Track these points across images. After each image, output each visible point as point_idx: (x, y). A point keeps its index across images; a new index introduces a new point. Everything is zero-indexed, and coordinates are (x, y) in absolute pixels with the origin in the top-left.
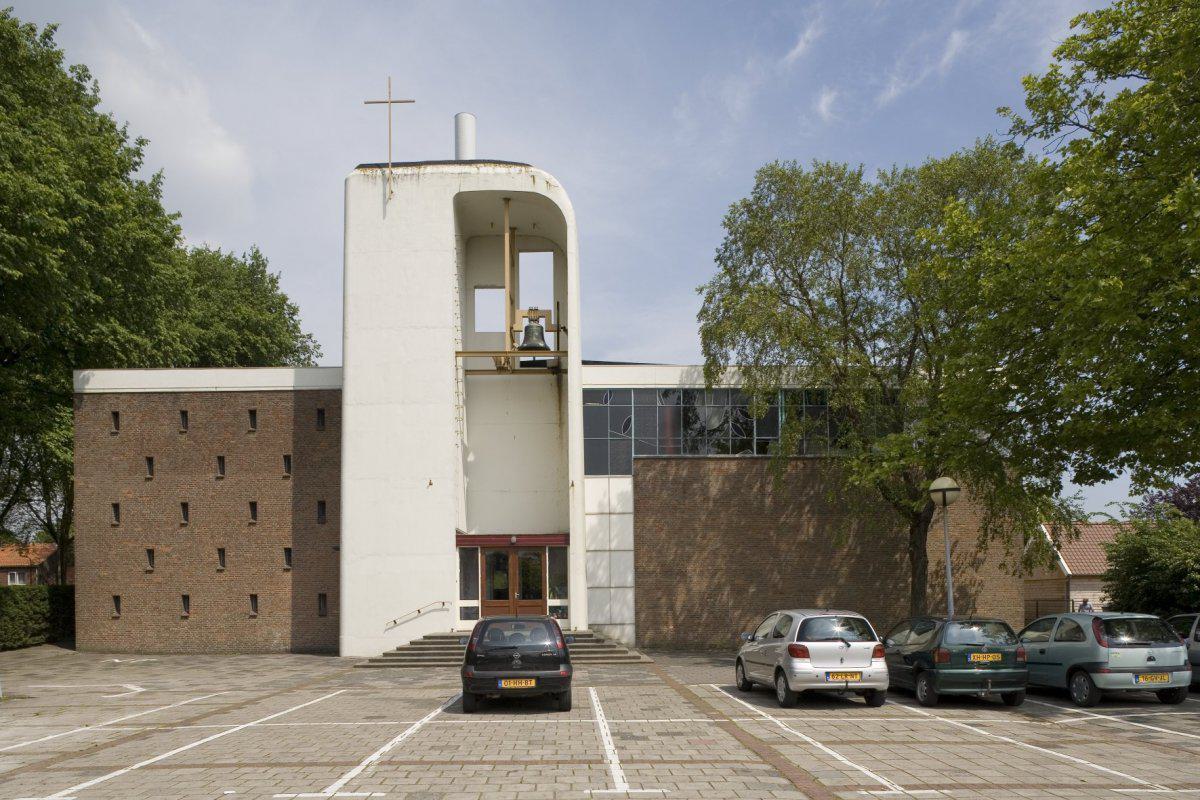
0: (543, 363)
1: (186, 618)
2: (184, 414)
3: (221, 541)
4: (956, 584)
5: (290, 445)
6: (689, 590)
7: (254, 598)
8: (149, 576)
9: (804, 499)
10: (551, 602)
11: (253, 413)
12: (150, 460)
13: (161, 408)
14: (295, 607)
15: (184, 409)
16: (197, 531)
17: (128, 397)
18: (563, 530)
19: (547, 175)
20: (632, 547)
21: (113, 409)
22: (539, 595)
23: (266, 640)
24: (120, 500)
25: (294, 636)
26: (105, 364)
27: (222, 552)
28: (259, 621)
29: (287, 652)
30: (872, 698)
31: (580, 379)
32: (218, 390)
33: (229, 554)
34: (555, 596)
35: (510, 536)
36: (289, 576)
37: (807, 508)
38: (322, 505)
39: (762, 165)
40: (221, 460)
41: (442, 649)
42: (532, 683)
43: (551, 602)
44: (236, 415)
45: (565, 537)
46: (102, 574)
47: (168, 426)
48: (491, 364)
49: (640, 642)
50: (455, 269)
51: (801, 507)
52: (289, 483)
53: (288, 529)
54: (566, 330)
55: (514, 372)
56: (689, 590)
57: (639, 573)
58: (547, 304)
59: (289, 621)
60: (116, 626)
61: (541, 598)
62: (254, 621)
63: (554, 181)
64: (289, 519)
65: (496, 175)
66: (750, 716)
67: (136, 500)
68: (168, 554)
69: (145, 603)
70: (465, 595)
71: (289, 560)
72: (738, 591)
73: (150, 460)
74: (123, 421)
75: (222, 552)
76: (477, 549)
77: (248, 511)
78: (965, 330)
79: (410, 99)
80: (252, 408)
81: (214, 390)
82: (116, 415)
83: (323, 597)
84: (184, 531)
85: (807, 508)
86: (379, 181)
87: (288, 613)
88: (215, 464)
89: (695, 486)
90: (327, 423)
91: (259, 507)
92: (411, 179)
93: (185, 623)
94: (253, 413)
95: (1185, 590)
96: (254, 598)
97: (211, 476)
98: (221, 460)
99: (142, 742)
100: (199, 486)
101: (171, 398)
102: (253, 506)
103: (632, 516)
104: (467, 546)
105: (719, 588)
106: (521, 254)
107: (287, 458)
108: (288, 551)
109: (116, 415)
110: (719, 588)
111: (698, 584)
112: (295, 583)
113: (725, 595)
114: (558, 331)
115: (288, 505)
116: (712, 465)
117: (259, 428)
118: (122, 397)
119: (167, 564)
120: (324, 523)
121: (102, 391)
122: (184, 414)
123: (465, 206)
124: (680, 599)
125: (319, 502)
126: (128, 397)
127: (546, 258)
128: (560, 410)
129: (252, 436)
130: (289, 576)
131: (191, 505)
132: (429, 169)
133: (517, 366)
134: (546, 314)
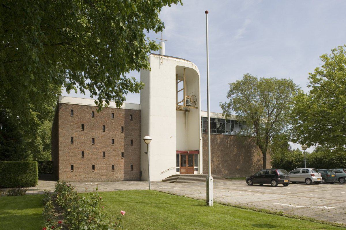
1: (94, 171)
3: (104, 150)
5: (124, 122)
8: (82, 159)
9: (235, 144)
10: (195, 167)
11: (113, 114)
13: (86, 110)
14: (125, 168)
15: (93, 111)
16: (97, 146)
17: (76, 106)
18: (198, 149)
19: (196, 66)
21: (72, 109)
22: (192, 166)
23: (116, 178)
24: (74, 136)
25: (124, 177)
28: (115, 172)
29: (122, 181)
33: (106, 153)
34: (196, 166)
36: (123, 160)
37: (235, 147)
41: (188, 178)
42: (287, 181)
43: (195, 167)
44: (108, 114)
46: (68, 158)
47: (89, 116)
51: (234, 146)
52: (123, 134)
53: (123, 147)
59: (123, 172)
60: (72, 174)
61: (193, 166)
62: (113, 172)
63: (196, 67)
64: (123, 144)
65: (185, 63)
67: (79, 137)
68: (88, 153)
69: (81, 167)
71: (123, 156)
72: (223, 165)
74: (75, 113)
76: (179, 154)
79: (167, 40)
80: (113, 112)
84: (93, 146)
85: (235, 147)
86: (159, 59)
87: (123, 170)
88: (102, 128)
89: (215, 141)
90: (133, 118)
91: (115, 140)
93: (93, 173)
94: (113, 114)
95: (292, 166)
98: (104, 126)
100: (98, 134)
102: (113, 140)
104: (178, 153)
105: (219, 164)
107: (122, 127)
108: (122, 153)
110: (219, 164)
112: (125, 162)
115: (123, 140)
116: (218, 136)
117: (115, 118)
118: (74, 106)
119: (88, 156)
121: (68, 103)
123: (178, 68)
125: (92, 138)
126: (76, 106)
128: (185, 120)
129: (113, 120)
130: (123, 160)
131: (95, 139)
132: (170, 58)
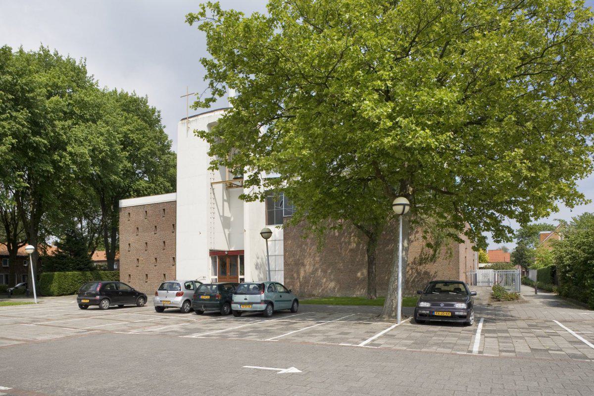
2: (146, 212)
4: (533, 275)
6: (305, 271)
7: (164, 275)
11: (164, 210)
12: (138, 228)
20: (283, 254)
26: (129, 197)
27: (156, 259)
30: (181, 311)
33: (158, 260)
35: (224, 251)
37: (353, 234)
39: (8, 45)
42: (88, 301)
45: (243, 251)
56: (305, 271)
57: (286, 264)
66: (583, 334)
72: (324, 271)
73: (138, 228)
75: (156, 259)
77: (162, 244)
82: (129, 214)
85: (353, 234)
94: (164, 210)
97: (153, 233)
99: (355, 329)
101: (143, 207)
103: (283, 241)
105: (317, 270)
109: (129, 214)
111: (309, 268)
113: (319, 273)
122: (146, 212)
124: (302, 274)
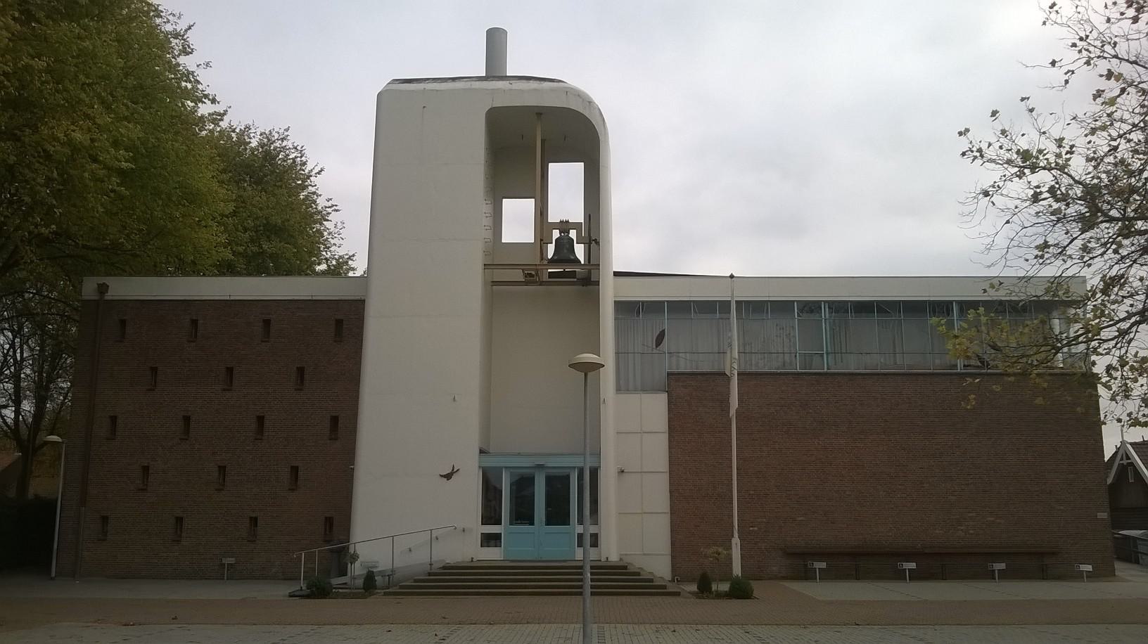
0: (573, 274)
12: (154, 370)
27: (222, 469)
31: (609, 292)
32: (314, 298)
38: (335, 420)
40: (230, 371)
48: (518, 275)
49: (679, 574)
50: (208, 81)
54: (597, 243)
55: (542, 283)
58: (577, 215)
70: (486, 520)
78: (1062, 194)
81: (310, 298)
83: (329, 522)
92: (1112, 422)
96: (254, 521)
102: (261, 420)
106: (550, 164)
114: (590, 244)
120: (336, 439)
127: (576, 170)
133: (546, 278)
134: (577, 226)
